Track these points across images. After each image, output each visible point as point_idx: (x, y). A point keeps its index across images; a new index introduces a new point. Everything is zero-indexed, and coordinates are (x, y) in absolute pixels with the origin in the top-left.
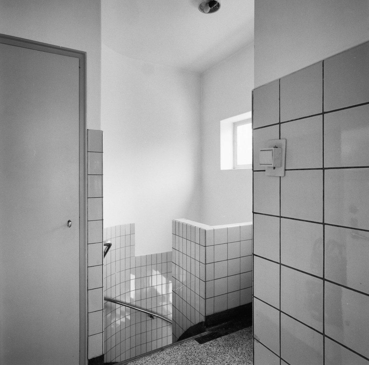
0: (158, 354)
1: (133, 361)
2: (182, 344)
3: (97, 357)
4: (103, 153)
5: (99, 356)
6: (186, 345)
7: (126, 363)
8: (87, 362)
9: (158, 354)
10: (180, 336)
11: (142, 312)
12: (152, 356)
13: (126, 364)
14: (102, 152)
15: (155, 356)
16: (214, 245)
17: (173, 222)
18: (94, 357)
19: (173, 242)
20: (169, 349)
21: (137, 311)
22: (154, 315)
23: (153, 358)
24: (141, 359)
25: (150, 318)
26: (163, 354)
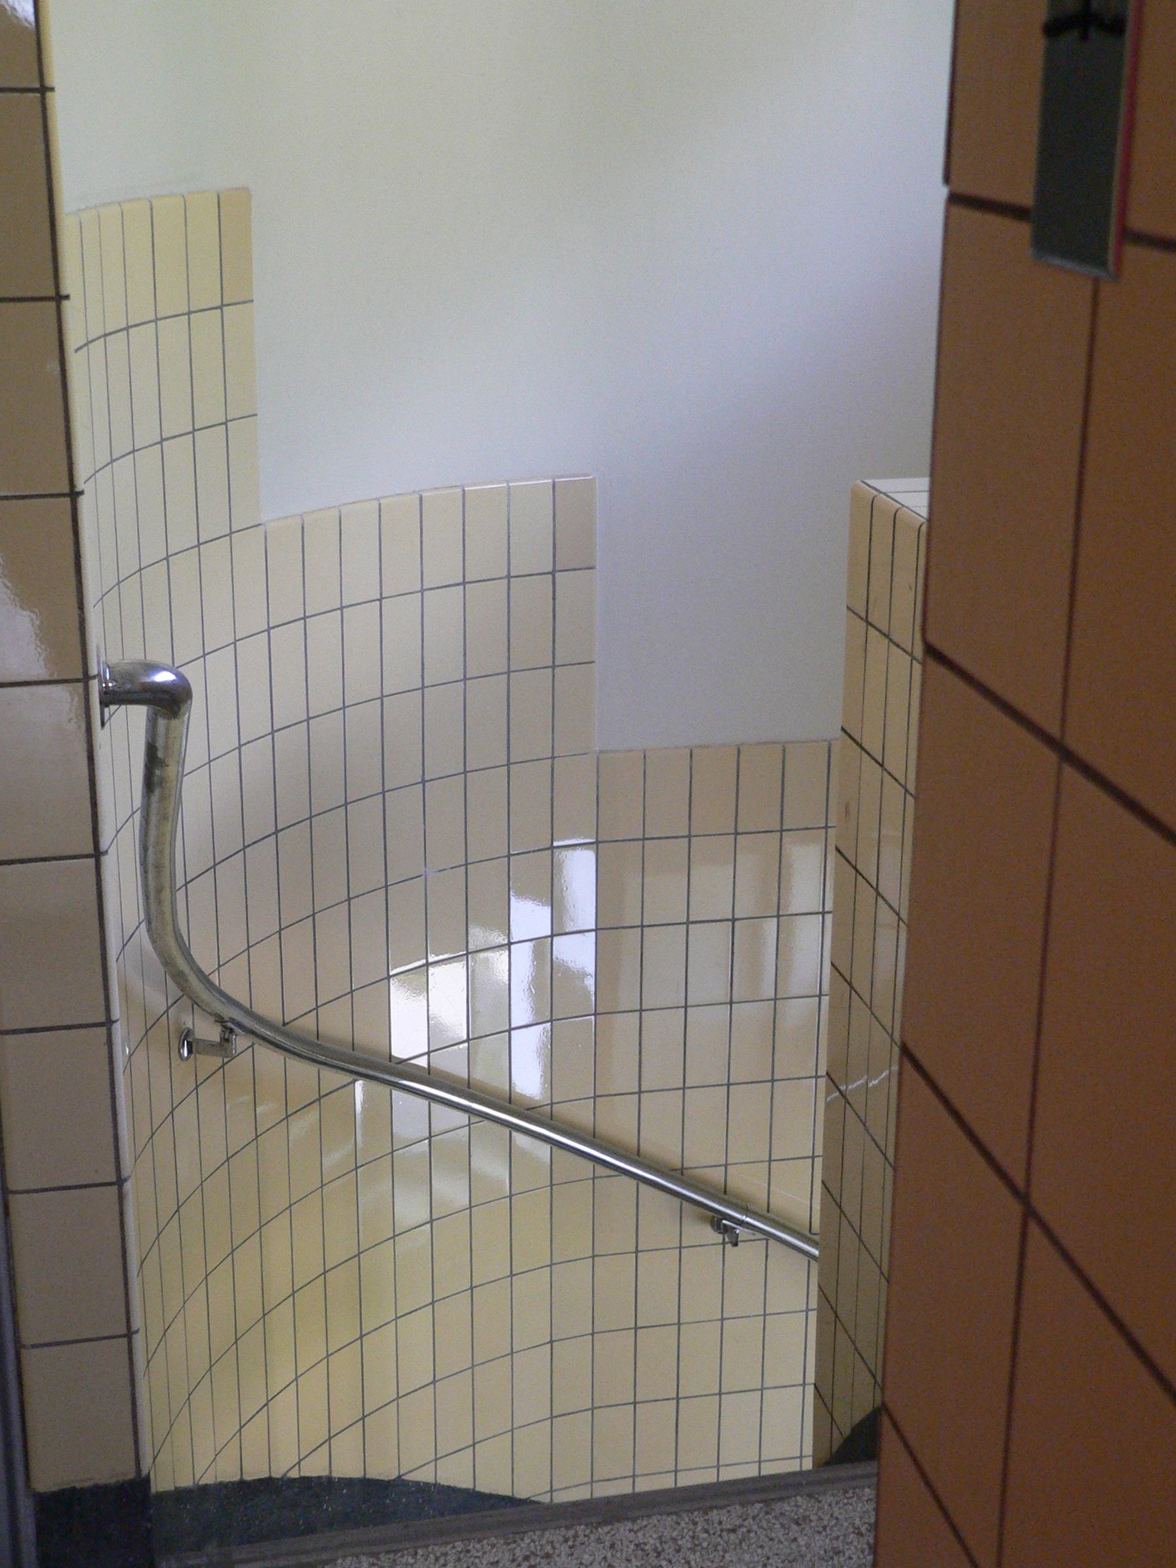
0: (576, 1536)
1: (374, 1549)
2: (781, 1499)
3: (97, 1487)
4: (66, 304)
5: (113, 1481)
6: (806, 1518)
7: (324, 1557)
8: (26, 1509)
9: (576, 1536)
10: (857, 1420)
11: (643, 1188)
12: (526, 1544)
13: (326, 1562)
14: (59, 298)
15: (548, 1549)
16: (644, 839)
17: (856, 496)
18: (78, 1486)
19: (176, 904)
20: (670, 1520)
21: (601, 1171)
22: (741, 1223)
23: (526, 1558)
24: (439, 1550)
25: (719, 1238)
26: (612, 1546)
